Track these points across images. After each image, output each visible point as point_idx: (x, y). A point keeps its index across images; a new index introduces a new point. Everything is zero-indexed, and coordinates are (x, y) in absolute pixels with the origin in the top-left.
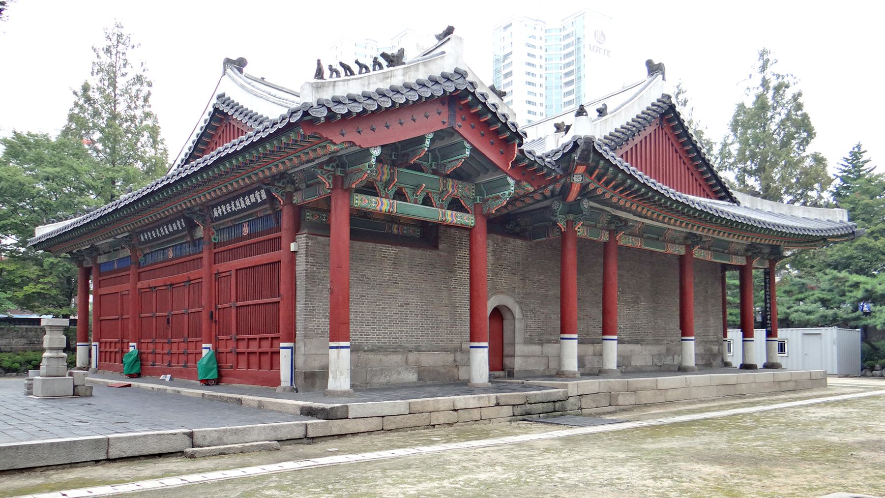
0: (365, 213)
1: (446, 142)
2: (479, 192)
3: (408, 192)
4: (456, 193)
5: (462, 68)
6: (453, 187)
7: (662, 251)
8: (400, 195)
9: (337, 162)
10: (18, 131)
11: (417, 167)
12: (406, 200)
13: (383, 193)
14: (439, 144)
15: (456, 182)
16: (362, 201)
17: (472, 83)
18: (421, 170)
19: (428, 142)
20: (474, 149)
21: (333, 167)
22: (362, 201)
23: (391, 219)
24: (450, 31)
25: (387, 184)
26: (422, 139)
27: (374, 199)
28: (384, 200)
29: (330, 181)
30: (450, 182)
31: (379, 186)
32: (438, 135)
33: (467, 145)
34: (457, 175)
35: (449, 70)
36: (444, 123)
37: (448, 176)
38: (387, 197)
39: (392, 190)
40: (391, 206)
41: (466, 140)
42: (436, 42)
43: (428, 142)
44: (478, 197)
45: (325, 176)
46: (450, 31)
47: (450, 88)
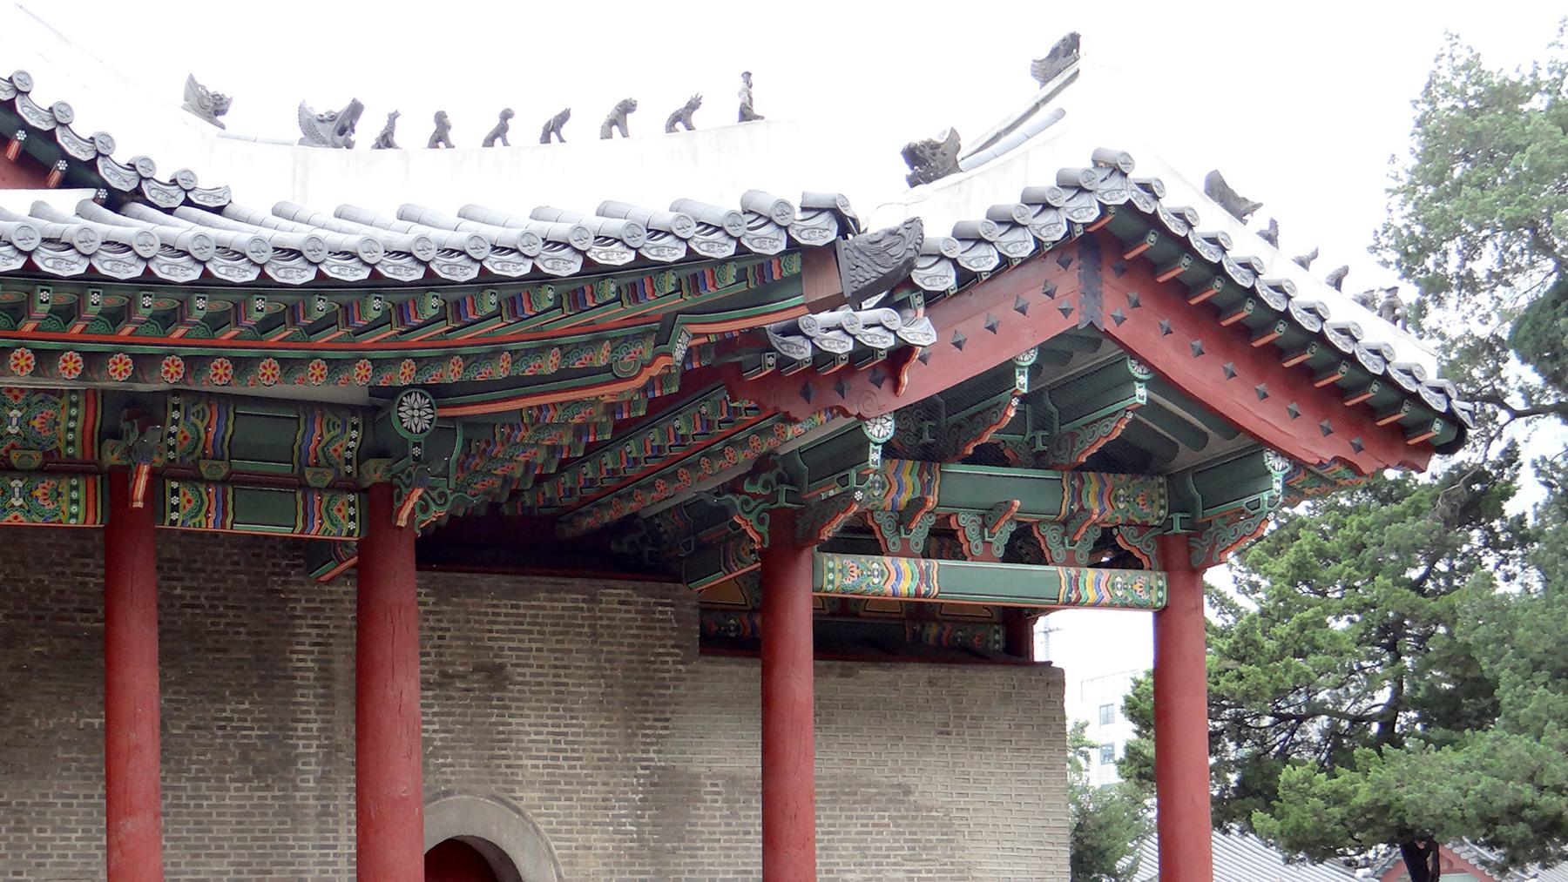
0: (844, 601)
1: (1082, 362)
2: (1178, 503)
3: (967, 523)
4: (1108, 514)
5: (1113, 146)
6: (1100, 497)
7: (285, 531)
8: (944, 542)
9: (779, 470)
10: (308, 106)
11: (990, 455)
12: (1041, 559)
13: (894, 542)
14: (1052, 376)
15: (1110, 479)
16: (847, 574)
17: (1146, 187)
18: (1003, 462)
19: (1022, 380)
20: (1160, 381)
21: (766, 485)
22: (847, 574)
23: (919, 610)
24: (1070, 47)
25: (904, 518)
26: (1005, 372)
27: (874, 563)
28: (904, 563)
29: (764, 529)
30: (1092, 483)
31: (883, 523)
32: (1051, 352)
33: (1137, 371)
34: (1109, 461)
35: (1079, 163)
36: (1066, 312)
37: (1080, 468)
38: (906, 553)
39: (920, 528)
40: (924, 576)
41: (1134, 355)
42: (1035, 90)
43: (1022, 380)
44: (1177, 517)
45: (753, 516)
46: (1070, 47)
47: (1086, 212)
